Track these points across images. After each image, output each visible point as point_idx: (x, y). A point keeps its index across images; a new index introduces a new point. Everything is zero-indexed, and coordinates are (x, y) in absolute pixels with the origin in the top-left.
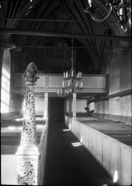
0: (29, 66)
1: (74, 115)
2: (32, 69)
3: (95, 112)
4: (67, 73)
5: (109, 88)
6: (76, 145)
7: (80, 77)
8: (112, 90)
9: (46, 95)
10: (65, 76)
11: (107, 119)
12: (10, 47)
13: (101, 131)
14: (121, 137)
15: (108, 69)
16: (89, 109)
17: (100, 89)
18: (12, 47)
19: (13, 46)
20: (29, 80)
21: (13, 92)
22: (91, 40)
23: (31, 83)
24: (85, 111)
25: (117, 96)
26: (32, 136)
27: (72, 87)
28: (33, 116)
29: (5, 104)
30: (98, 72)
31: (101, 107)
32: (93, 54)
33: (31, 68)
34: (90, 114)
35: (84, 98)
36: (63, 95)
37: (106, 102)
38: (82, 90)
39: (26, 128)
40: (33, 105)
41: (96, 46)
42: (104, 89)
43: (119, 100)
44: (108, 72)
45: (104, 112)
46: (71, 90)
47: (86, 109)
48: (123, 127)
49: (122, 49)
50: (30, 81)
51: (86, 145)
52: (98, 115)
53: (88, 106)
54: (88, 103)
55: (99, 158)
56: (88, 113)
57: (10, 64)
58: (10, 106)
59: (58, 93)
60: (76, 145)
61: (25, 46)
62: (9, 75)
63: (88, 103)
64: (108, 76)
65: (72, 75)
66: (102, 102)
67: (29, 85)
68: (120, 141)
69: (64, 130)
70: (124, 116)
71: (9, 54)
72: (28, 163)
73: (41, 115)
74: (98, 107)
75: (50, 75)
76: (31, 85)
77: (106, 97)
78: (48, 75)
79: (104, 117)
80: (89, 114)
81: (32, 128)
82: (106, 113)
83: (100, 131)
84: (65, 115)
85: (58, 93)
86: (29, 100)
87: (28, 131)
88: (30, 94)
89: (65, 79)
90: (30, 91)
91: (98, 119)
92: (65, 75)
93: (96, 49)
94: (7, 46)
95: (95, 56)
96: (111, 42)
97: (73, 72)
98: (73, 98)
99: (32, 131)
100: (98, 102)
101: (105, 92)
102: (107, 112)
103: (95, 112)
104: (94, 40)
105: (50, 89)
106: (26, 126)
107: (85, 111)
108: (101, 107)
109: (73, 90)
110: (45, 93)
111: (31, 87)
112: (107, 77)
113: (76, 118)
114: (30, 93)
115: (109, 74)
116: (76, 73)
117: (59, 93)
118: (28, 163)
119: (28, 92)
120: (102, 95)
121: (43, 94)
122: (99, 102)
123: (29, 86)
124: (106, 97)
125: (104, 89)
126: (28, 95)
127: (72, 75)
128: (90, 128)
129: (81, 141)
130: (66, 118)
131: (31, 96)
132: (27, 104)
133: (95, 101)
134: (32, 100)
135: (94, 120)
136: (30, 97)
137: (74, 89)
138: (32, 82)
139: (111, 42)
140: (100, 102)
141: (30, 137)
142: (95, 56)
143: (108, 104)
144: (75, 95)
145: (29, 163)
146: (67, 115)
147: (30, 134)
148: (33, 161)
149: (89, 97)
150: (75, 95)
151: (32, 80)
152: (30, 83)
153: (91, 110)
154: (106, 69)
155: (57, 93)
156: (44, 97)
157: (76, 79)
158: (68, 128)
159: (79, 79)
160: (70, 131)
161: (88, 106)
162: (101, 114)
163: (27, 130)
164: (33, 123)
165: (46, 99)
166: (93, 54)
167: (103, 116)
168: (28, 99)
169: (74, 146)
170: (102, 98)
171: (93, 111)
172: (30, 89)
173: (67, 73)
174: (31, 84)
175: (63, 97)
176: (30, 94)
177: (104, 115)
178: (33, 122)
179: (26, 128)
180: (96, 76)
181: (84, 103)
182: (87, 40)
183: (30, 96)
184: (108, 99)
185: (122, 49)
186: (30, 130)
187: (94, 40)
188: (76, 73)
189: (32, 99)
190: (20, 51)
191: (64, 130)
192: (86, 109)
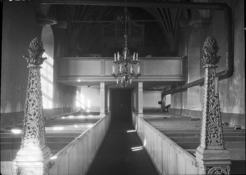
0: (32, 43)
1: (141, 111)
2: (36, 47)
3: (172, 107)
4: (118, 54)
5: (187, 77)
6: (135, 149)
7: (137, 59)
8: (191, 77)
9: (102, 85)
10: (117, 59)
11: (185, 115)
12: (49, 23)
13: (163, 132)
14: (191, 138)
15: (186, 49)
16: (164, 103)
17: (175, 76)
18: (53, 23)
19: (53, 21)
20: (31, 61)
21: (59, 81)
22: (164, 9)
23: (35, 66)
24: (159, 106)
25: (196, 85)
26: (36, 137)
27: (125, 73)
28: (37, 110)
29: (48, 98)
30: (174, 54)
31: (178, 100)
32: (167, 29)
33: (35, 46)
34: (166, 110)
35: (154, 88)
36: (124, 85)
37: (184, 93)
38: (139, 77)
39: (28, 125)
40: (37, 96)
41: (170, 18)
42: (180, 76)
43: (198, 91)
44: (186, 54)
45: (182, 107)
46: (124, 77)
47: (160, 103)
48: (196, 126)
49: (201, 21)
50: (33, 63)
51: (149, 150)
52: (175, 110)
53: (162, 99)
54: (163, 96)
55: (159, 167)
56: (163, 109)
57: (53, 46)
58: (55, 100)
59: (117, 83)
60: (135, 149)
61: (74, 21)
62: (53, 60)
63: (163, 96)
64: (186, 58)
65: (125, 58)
66: (179, 94)
67: (31, 68)
68: (178, 144)
69: (128, 131)
70: (235, 114)
71: (51, 33)
72: (30, 172)
73: (98, 112)
74: (174, 100)
75: (107, 59)
76: (35, 68)
77: (183, 87)
78: (104, 59)
79: (181, 113)
80: (164, 109)
81: (36, 126)
82: (183, 108)
83: (161, 131)
84: (133, 112)
85: (117, 83)
86: (32, 88)
87: (31, 130)
88: (33, 81)
89: (116, 63)
90: (33, 77)
91: (171, 116)
92: (117, 56)
93: (171, 22)
94: (47, 21)
95: (170, 32)
96: (189, 11)
97: (126, 53)
98: (139, 89)
99: (36, 130)
100: (174, 94)
101: (182, 80)
102: (185, 106)
103: (172, 107)
104: (168, 9)
105: (107, 78)
106: (28, 124)
107: (159, 106)
108: (178, 100)
109: (127, 77)
110: (101, 83)
111: (35, 71)
112: (185, 61)
113: (142, 115)
114: (33, 79)
115: (186, 55)
116: (130, 54)
117: (119, 82)
118: (30, 172)
119: (30, 78)
120: (178, 84)
121: (98, 84)
122: (175, 94)
123: (32, 70)
124: (183, 87)
125: (180, 76)
126: (31, 82)
127: (125, 58)
128: (152, 127)
129: (145, 144)
130: (133, 115)
131: (35, 83)
132: (30, 94)
133: (172, 92)
134: (36, 89)
135: (166, 118)
136: (33, 85)
137: (128, 76)
138: (36, 63)
139: (189, 11)
140: (177, 93)
141: (34, 138)
142: (170, 32)
143: (186, 96)
144: (140, 85)
145: (32, 172)
146: (134, 111)
147: (33, 134)
148: (37, 169)
149: (163, 88)
150: (140, 85)
151: (35, 61)
152: (32, 65)
153: (167, 105)
154: (184, 49)
155: (116, 82)
156: (99, 88)
157: (131, 62)
158: (134, 129)
159: (135, 63)
160: (136, 132)
161: (162, 99)
162: (179, 109)
163: (29, 128)
164: (38, 120)
165: (103, 90)
166: (167, 29)
167: (180, 112)
168: (31, 87)
169: (133, 150)
170: (178, 88)
171: (169, 106)
172: (33, 74)
173: (118, 54)
174: (33, 66)
175: (124, 87)
176: (33, 81)
177: (181, 110)
178: (37, 118)
179: (28, 125)
180: (169, 58)
181: (157, 95)
182: (158, 9)
183: (33, 83)
184: (186, 90)
185: (201, 21)
186: (33, 128)
187: (168, 9)
188: (130, 54)
189: (36, 87)
190: (65, 28)
191: (128, 131)
192: (160, 103)
